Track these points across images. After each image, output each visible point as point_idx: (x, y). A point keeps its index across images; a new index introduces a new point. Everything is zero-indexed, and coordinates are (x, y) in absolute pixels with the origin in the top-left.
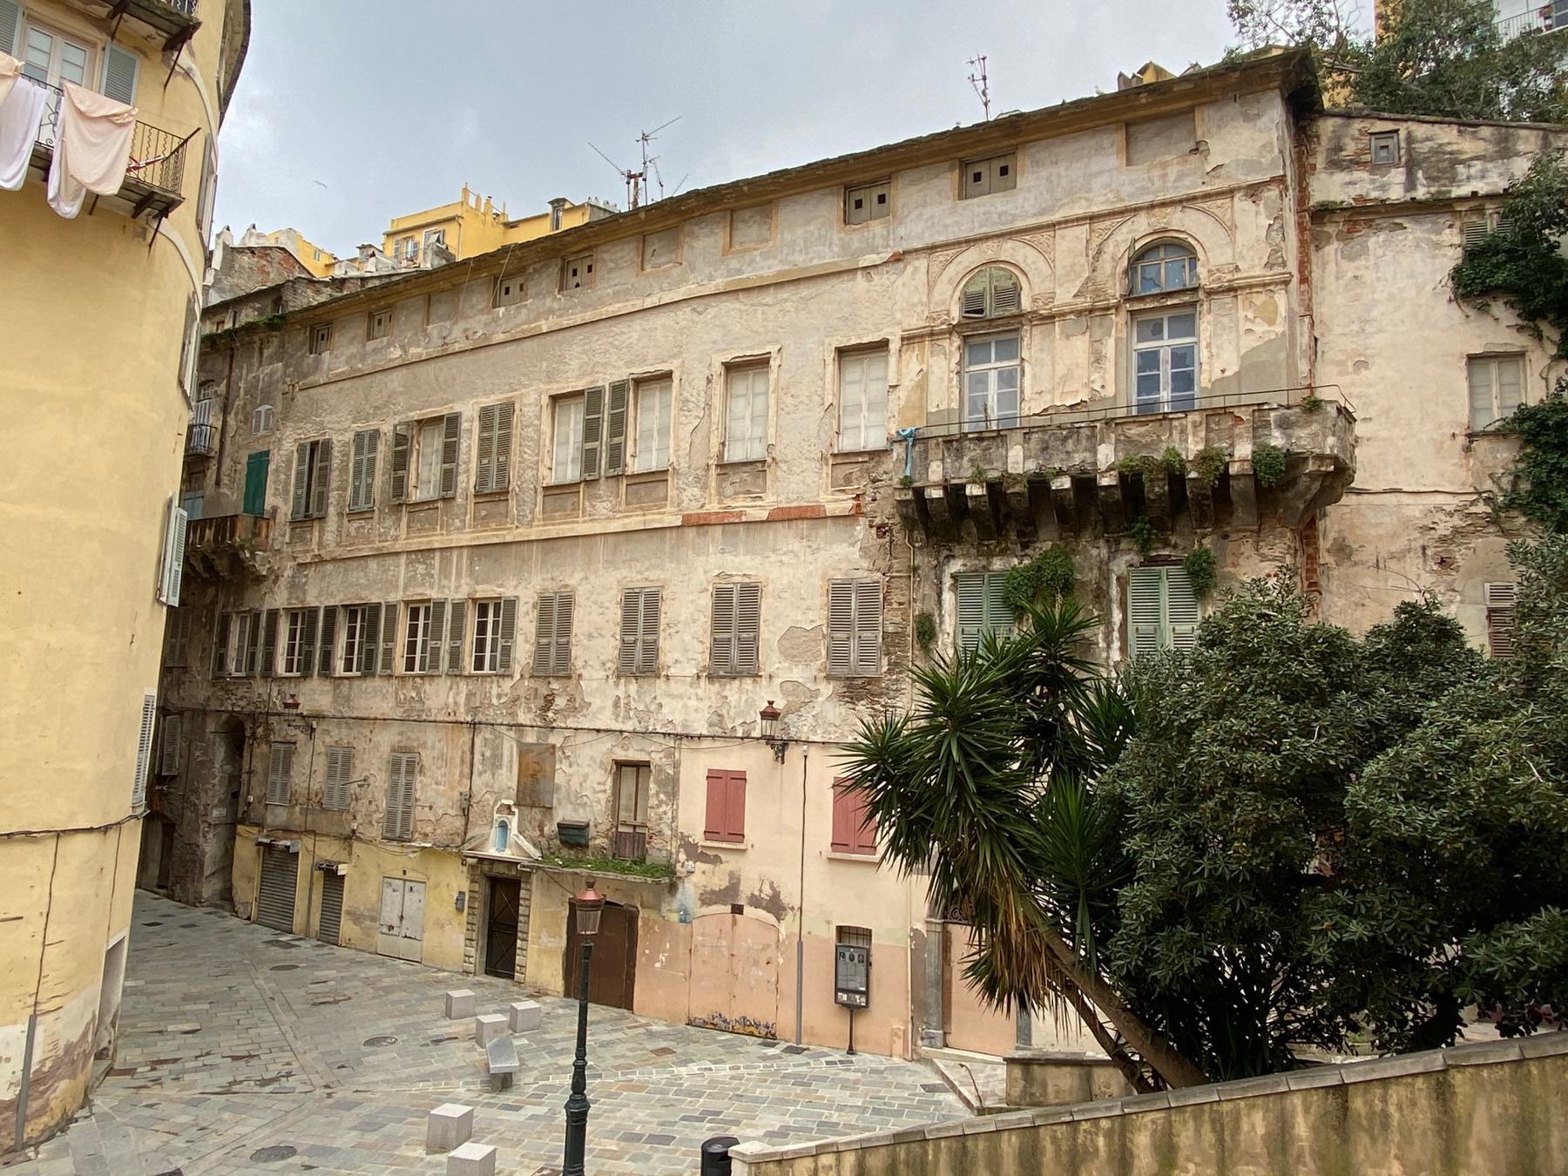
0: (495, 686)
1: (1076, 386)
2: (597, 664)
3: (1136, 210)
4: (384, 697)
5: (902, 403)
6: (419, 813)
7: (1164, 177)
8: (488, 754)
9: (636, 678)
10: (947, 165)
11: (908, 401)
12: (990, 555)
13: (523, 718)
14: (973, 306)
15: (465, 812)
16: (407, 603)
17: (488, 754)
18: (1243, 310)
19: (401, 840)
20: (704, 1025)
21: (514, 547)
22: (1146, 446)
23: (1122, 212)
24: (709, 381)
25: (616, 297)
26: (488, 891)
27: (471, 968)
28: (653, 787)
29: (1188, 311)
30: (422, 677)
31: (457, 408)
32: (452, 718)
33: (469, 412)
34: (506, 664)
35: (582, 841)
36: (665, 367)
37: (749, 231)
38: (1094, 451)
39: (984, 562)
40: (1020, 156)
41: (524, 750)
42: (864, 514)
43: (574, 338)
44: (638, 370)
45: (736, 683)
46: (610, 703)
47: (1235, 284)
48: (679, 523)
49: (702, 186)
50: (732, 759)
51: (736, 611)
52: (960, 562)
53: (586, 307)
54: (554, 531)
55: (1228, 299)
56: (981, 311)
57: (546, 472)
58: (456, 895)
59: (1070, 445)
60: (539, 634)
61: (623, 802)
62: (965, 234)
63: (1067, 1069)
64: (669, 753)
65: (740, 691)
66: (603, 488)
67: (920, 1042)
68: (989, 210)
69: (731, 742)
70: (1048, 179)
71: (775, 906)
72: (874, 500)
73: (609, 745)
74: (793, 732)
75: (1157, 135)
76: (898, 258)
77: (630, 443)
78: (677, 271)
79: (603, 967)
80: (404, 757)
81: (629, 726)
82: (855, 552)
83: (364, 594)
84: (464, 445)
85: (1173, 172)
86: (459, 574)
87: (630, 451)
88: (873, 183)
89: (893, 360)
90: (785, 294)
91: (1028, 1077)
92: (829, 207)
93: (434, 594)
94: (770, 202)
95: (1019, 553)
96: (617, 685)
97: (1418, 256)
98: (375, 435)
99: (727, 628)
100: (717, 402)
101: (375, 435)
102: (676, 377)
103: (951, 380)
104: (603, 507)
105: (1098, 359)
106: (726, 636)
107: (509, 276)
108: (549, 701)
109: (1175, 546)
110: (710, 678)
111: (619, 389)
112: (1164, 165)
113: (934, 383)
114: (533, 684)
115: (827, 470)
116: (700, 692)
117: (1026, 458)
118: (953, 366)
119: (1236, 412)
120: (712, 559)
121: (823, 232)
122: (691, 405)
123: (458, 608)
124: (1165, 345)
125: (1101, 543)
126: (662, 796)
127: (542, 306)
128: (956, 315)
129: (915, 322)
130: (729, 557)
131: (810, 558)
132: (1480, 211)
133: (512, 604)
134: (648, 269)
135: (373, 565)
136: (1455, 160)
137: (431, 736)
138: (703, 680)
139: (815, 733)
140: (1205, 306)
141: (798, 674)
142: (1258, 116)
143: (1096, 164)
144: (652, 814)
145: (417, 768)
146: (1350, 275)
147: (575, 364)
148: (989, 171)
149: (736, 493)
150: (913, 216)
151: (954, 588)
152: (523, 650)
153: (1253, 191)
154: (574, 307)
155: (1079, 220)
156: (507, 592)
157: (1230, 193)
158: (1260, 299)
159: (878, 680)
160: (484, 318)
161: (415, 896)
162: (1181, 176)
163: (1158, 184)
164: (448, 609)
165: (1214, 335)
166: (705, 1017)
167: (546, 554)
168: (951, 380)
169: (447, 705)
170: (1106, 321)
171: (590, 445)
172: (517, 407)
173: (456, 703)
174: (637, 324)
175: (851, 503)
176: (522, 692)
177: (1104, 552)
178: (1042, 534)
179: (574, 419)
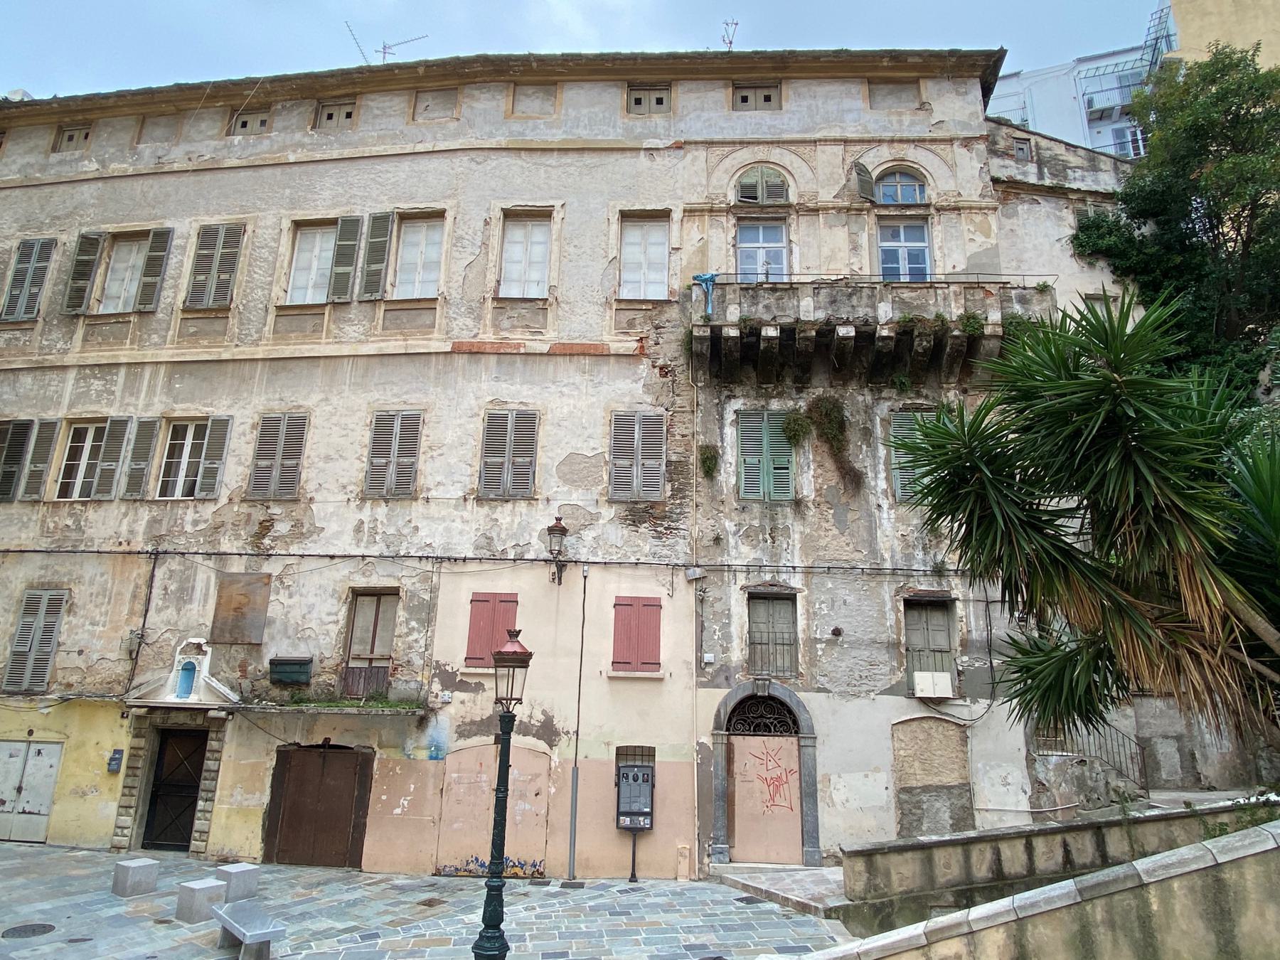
0: (190, 512)
1: (839, 266)
2: (334, 487)
3: (880, 141)
4: (25, 526)
5: (684, 263)
6: (60, 660)
7: (900, 122)
8: (173, 587)
9: (387, 501)
10: (721, 83)
11: (689, 263)
12: (769, 397)
13: (226, 546)
14: (747, 192)
15: (133, 656)
16: (71, 422)
17: (173, 587)
18: (965, 224)
19: (28, 693)
20: (456, 873)
21: (230, 366)
22: (918, 307)
23: (869, 141)
24: (487, 223)
25: (381, 139)
26: (157, 744)
27: (124, 841)
28: (402, 614)
29: (919, 223)
30: (84, 503)
31: (168, 224)
32: (125, 548)
33: (185, 231)
34: (210, 487)
35: (303, 678)
36: (438, 206)
37: (531, 103)
38: (874, 308)
39: (763, 403)
40: (784, 87)
41: (225, 581)
42: (648, 356)
43: (327, 171)
44: (405, 206)
45: (509, 506)
46: (350, 527)
47: (961, 204)
48: (449, 349)
49: (491, 52)
50: (500, 582)
51: (510, 436)
52: (741, 401)
53: (344, 145)
54: (287, 351)
55: (954, 215)
56: (756, 198)
57: (282, 294)
58: (108, 755)
59: (854, 300)
60: (259, 455)
61: (357, 633)
62: (737, 135)
63: (909, 855)
64: (426, 577)
65: (513, 513)
66: (354, 312)
67: (706, 860)
68: (755, 121)
69: (502, 565)
70: (809, 108)
71: (548, 732)
72: (657, 344)
73: (346, 572)
74: (571, 555)
75: (890, 93)
76: (679, 146)
77: (391, 271)
78: (453, 125)
79: (320, 815)
80: (46, 595)
81: (375, 551)
82: (639, 388)
83: (7, 411)
84: (173, 261)
85: (907, 119)
86: (152, 388)
87: (390, 278)
88: (651, 87)
89: (675, 227)
90: (569, 159)
91: (871, 869)
92: (613, 98)
93: (113, 412)
94: (555, 83)
95: (794, 396)
96: (360, 508)
97: (1048, 224)
98: (48, 246)
99: (501, 452)
100: (495, 242)
101: (48, 246)
102: (449, 216)
103: (728, 250)
104: (352, 331)
105: (855, 248)
106: (500, 460)
107: (251, 110)
108: (266, 527)
109: (926, 397)
110: (479, 500)
111: (380, 223)
112: (900, 114)
113: (717, 250)
114: (245, 508)
115: (610, 314)
116: (466, 515)
117: (815, 309)
118: (730, 239)
119: (987, 286)
120: (484, 386)
121: (607, 115)
122: (466, 243)
123: (147, 429)
124: (903, 246)
125: (866, 391)
126: (413, 624)
127: (289, 136)
128: (732, 198)
129: (696, 199)
130: (504, 385)
131: (591, 390)
132: (1083, 201)
133: (222, 425)
134: (420, 120)
135: (27, 380)
136: (1066, 167)
137: (90, 569)
138: (470, 504)
139: (596, 555)
140: (936, 219)
141: (577, 497)
142: (966, 93)
143: (848, 103)
144: (399, 644)
145: (64, 607)
146: (1008, 228)
147: (326, 194)
148: (755, 96)
149: (514, 327)
150: (692, 116)
151: (736, 422)
152: (235, 470)
153: (967, 142)
154: (331, 143)
155: (836, 141)
156: (218, 410)
157: (950, 141)
158: (978, 218)
159: (664, 503)
160: (213, 143)
161: (45, 760)
162: (912, 124)
163: (896, 126)
164: (131, 432)
165: (944, 240)
166: (457, 863)
167: (275, 373)
168: (728, 250)
169: (118, 534)
170: (860, 219)
171: (341, 270)
172: (249, 228)
173: (131, 532)
174: (406, 164)
175: (635, 345)
176: (228, 518)
177: (869, 398)
178: (815, 381)
179: (323, 247)
